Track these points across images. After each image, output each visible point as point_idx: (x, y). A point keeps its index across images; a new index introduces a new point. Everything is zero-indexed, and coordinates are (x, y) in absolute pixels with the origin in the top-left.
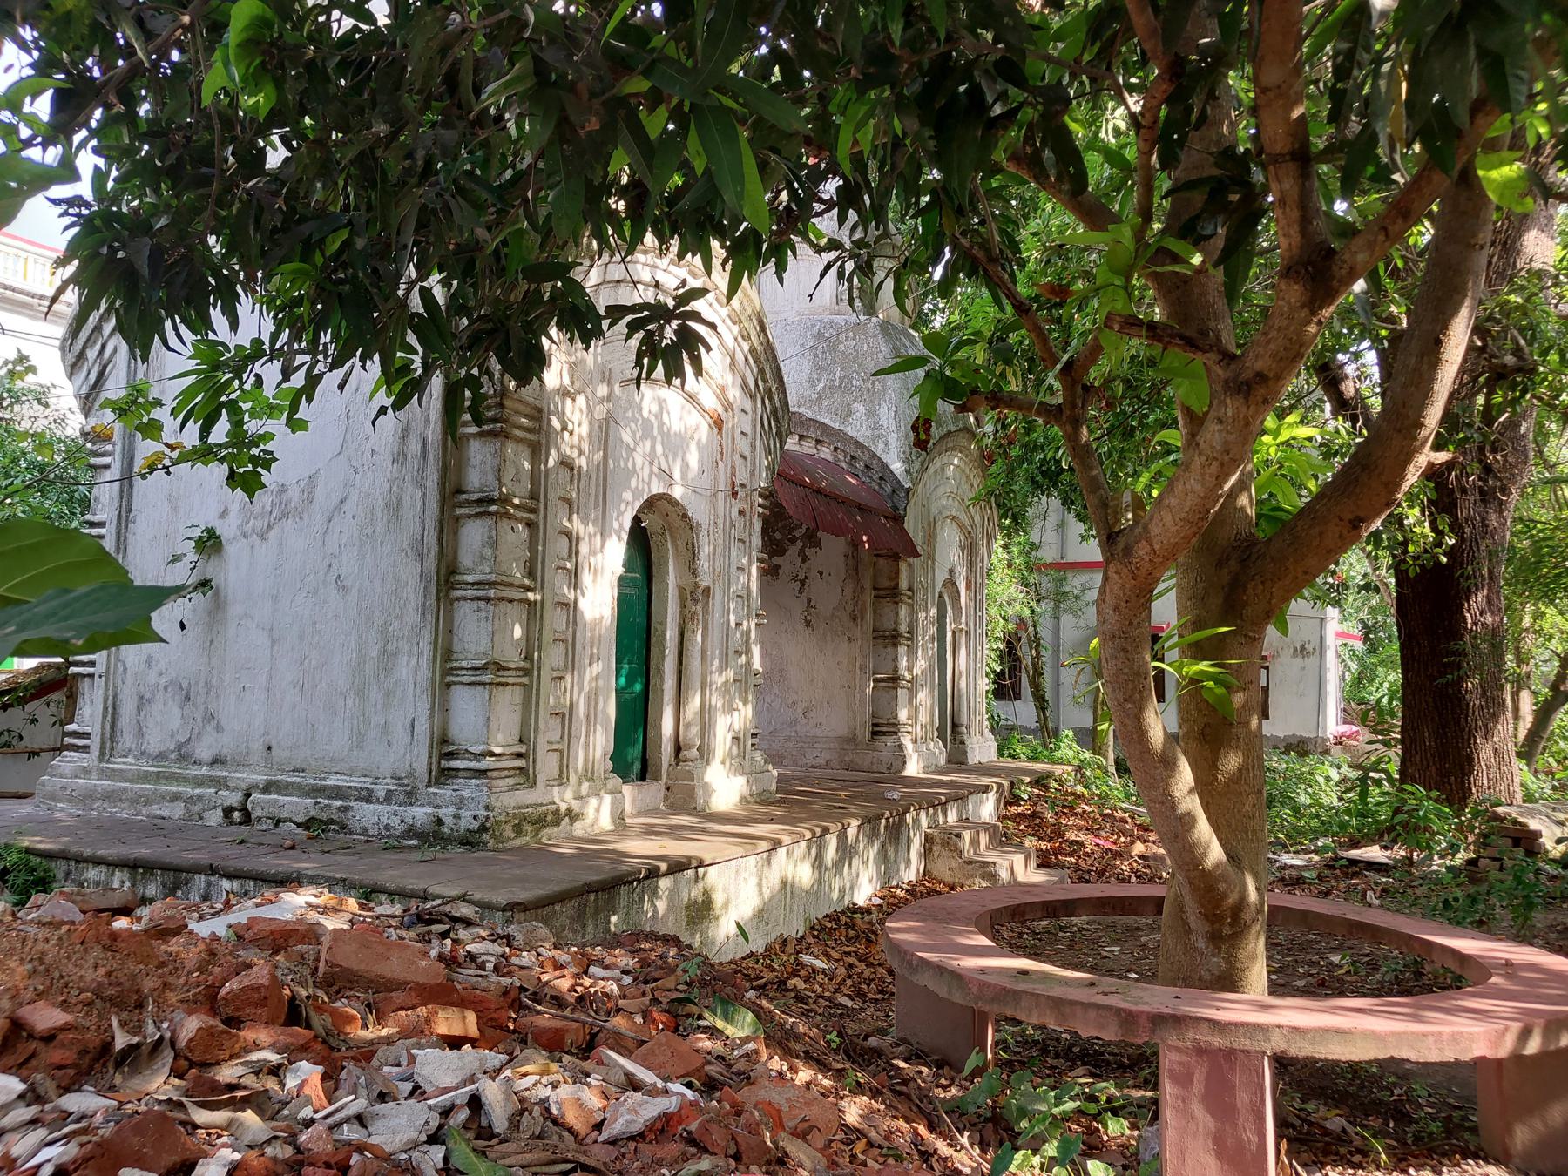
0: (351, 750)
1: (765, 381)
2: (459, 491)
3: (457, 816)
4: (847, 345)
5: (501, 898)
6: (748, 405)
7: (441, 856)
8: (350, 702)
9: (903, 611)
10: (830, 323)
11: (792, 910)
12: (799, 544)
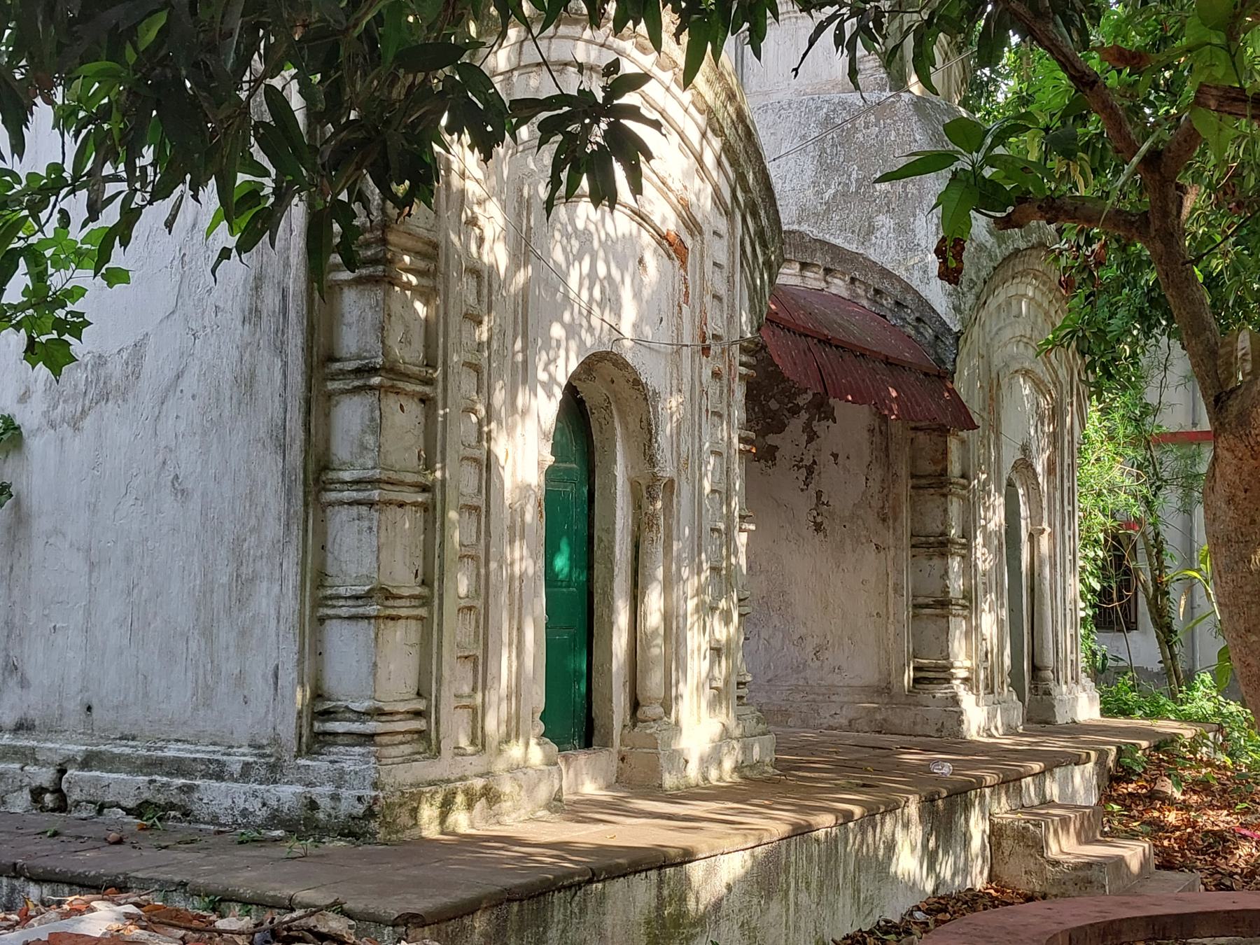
0: (196, 709)
1: (746, 190)
2: (332, 359)
3: (335, 798)
4: (867, 133)
5: (393, 907)
6: (722, 225)
7: (315, 851)
8: (193, 645)
9: (955, 507)
10: (842, 103)
11: (797, 929)
12: (804, 416)
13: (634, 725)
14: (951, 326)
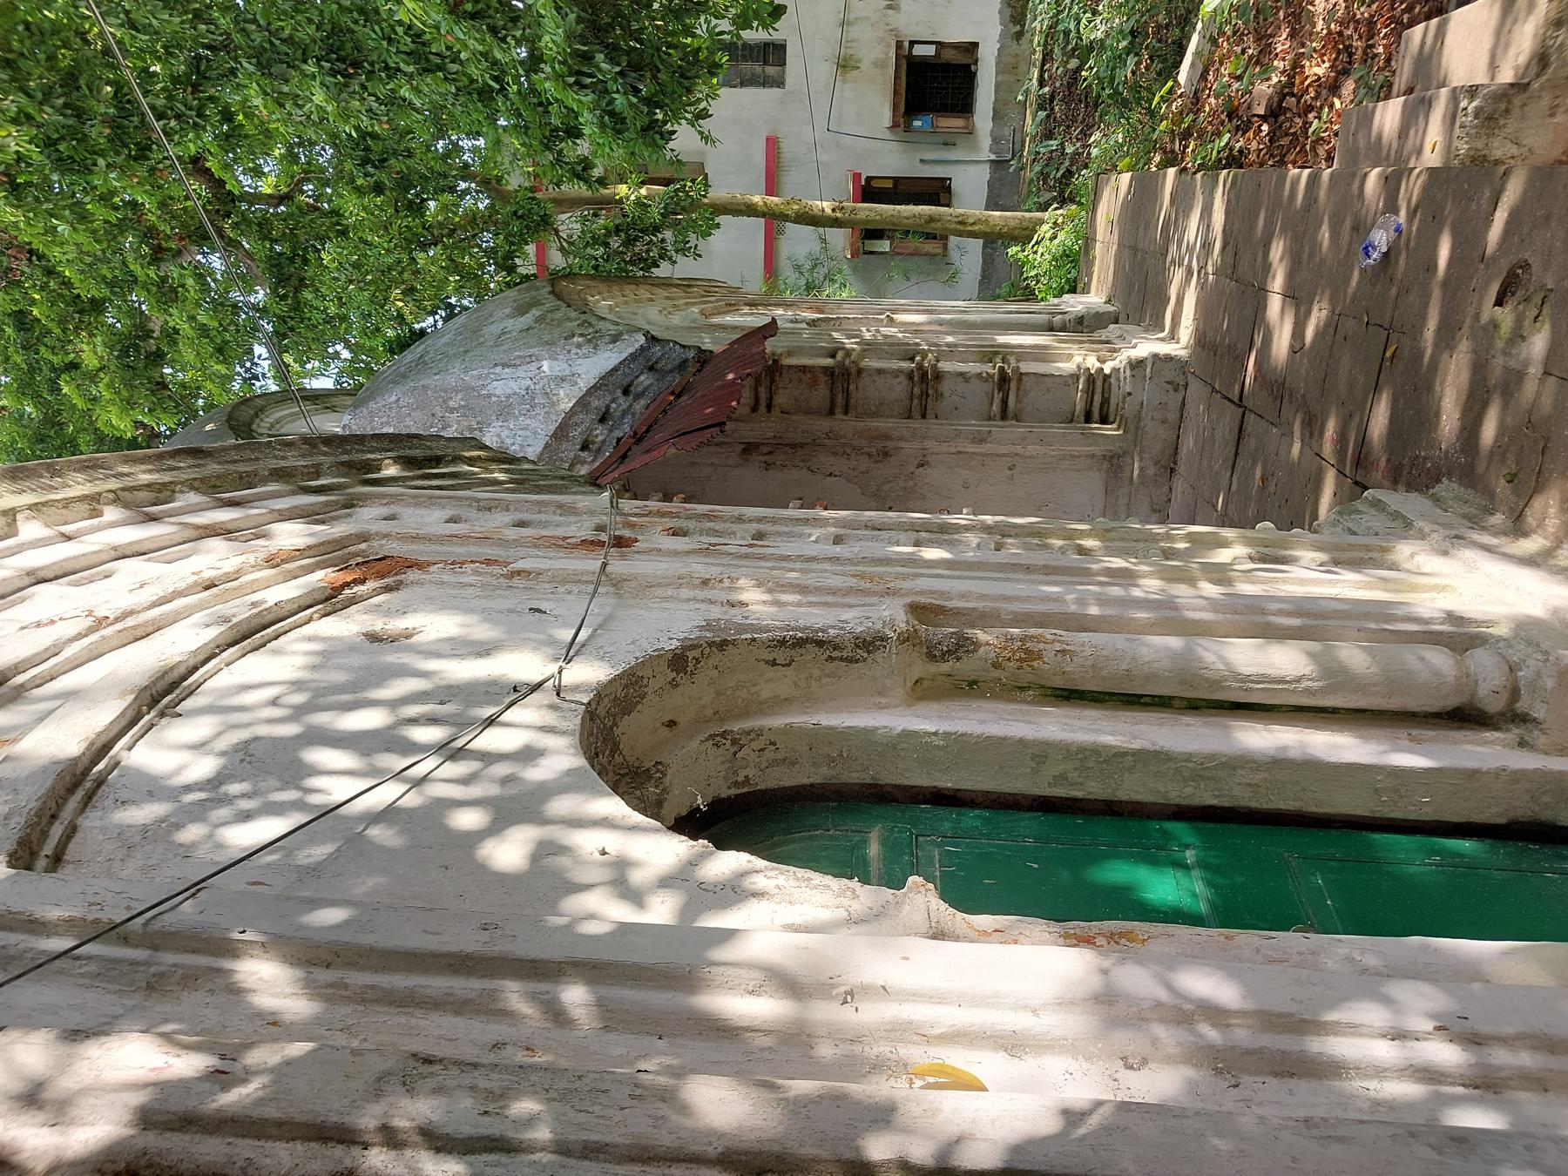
13: (1523, 719)
14: (637, 346)
